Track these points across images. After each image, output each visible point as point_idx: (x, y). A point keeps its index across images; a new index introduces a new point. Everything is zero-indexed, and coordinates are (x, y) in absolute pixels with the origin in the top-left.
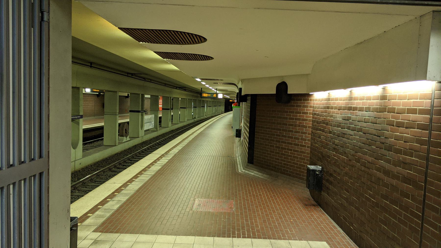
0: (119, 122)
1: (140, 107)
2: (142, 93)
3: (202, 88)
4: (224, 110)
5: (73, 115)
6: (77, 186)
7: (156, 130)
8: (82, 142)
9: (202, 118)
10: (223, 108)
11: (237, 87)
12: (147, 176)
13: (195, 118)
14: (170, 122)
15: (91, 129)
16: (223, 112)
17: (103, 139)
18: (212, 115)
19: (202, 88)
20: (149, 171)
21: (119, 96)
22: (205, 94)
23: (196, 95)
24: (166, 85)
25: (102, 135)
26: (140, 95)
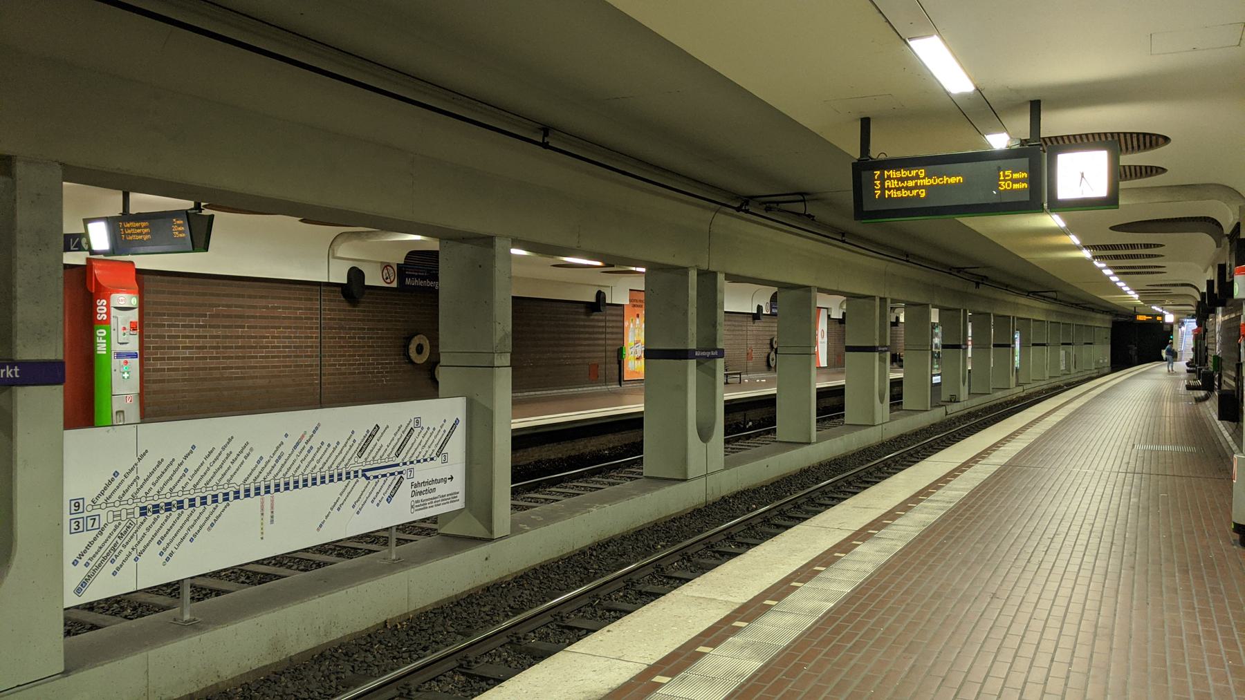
0: (891, 378)
1: (877, 337)
2: (704, 267)
3: (866, 123)
4: (1108, 360)
5: (976, 346)
6: (635, 578)
7: (478, 530)
8: (723, 435)
9: (999, 396)
10: (1102, 353)
11: (1199, 291)
12: (940, 504)
13: (954, 400)
14: (964, 384)
15: (741, 402)
16: (1106, 370)
17: (843, 415)
18: (1053, 380)
19: (866, 123)
20: (894, 527)
21: (513, 297)
22: (904, 173)
23: (955, 283)
24: (1008, 289)
25: (638, 448)
26: (693, 276)
